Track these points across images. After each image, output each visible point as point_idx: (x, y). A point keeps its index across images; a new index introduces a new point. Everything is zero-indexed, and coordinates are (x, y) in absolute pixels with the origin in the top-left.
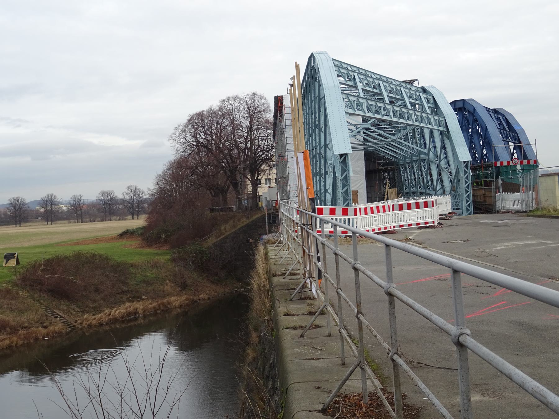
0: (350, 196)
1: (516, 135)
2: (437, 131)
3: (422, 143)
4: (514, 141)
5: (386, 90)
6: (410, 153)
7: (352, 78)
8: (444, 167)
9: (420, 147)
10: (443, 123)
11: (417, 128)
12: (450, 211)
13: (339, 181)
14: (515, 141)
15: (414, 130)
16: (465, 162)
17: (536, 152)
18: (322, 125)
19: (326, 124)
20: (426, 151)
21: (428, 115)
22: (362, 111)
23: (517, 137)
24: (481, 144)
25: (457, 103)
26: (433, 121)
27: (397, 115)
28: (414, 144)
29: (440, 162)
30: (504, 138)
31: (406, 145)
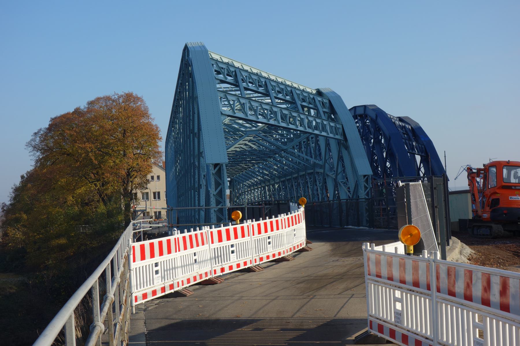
0: (225, 215)
1: (423, 147)
2: (333, 139)
3: (318, 153)
4: (420, 153)
5: (299, 98)
6: (304, 165)
7: (233, 75)
8: (342, 182)
9: (315, 159)
10: (341, 130)
11: (312, 136)
12: (304, 246)
13: (212, 195)
14: (422, 153)
15: (308, 139)
16: (365, 176)
17: (446, 166)
18: (196, 130)
19: (199, 129)
20: (321, 163)
21: (322, 121)
22: (295, 125)
23: (424, 149)
24: (385, 157)
25: (357, 109)
26: (328, 128)
27: (286, 120)
28: (308, 155)
29: (336, 176)
30: (419, 153)
31: (299, 156)
